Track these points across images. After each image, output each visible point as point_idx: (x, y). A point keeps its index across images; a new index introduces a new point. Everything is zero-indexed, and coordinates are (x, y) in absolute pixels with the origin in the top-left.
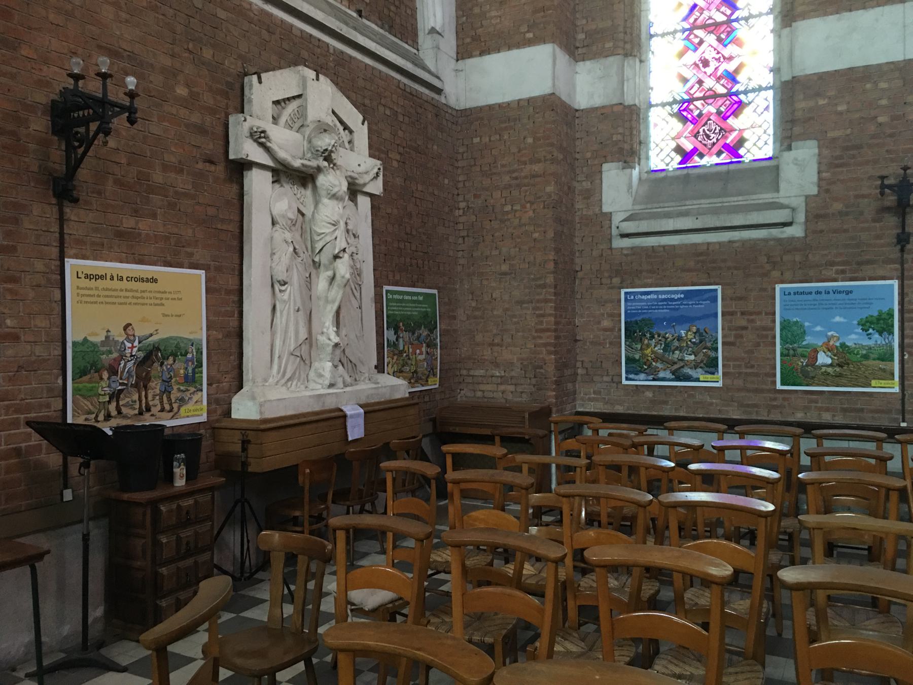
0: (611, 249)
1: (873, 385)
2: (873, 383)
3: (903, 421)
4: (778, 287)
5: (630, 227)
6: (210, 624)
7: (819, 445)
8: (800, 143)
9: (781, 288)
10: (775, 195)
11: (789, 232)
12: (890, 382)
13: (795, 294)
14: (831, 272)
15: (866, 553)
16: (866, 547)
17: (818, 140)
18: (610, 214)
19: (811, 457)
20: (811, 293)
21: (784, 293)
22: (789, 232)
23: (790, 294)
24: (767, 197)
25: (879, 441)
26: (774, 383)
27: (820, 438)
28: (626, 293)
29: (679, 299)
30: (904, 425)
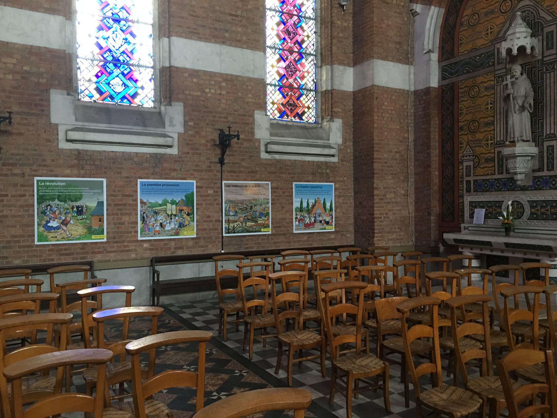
0: (58, 149)
1: (93, 238)
2: (262, 230)
3: (222, 250)
4: (294, 183)
5: (74, 135)
6: (411, 383)
7: (241, 262)
8: (176, 103)
9: (140, 182)
10: (163, 130)
11: (168, 151)
12: (102, 236)
13: (310, 187)
14: (174, 174)
15: (80, 337)
16: (236, 313)
17: (342, 118)
18: (57, 125)
19: (37, 285)
20: (160, 185)
21: (143, 184)
22: (168, 151)
23: (145, 185)
24: (159, 131)
25: (27, 275)
26: (34, 241)
27: (284, 256)
28: (38, 181)
29: (63, 186)
30: (223, 252)
